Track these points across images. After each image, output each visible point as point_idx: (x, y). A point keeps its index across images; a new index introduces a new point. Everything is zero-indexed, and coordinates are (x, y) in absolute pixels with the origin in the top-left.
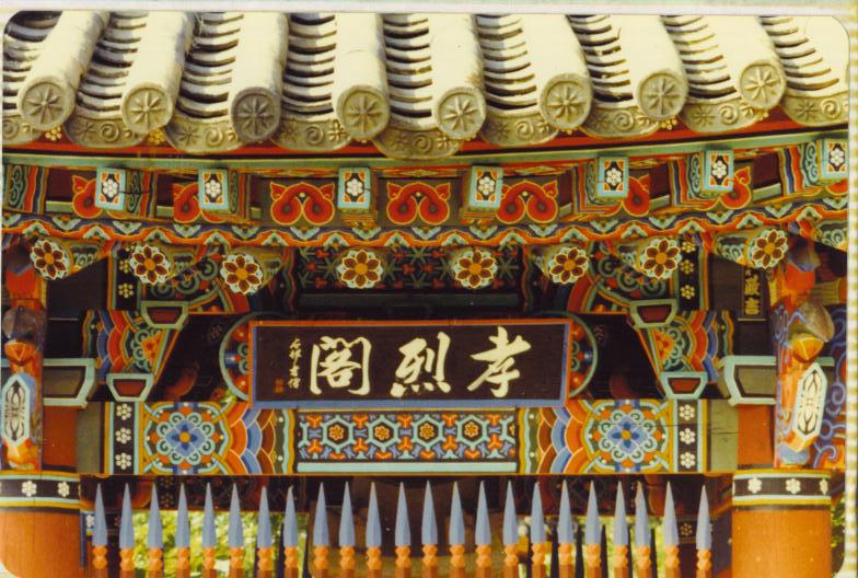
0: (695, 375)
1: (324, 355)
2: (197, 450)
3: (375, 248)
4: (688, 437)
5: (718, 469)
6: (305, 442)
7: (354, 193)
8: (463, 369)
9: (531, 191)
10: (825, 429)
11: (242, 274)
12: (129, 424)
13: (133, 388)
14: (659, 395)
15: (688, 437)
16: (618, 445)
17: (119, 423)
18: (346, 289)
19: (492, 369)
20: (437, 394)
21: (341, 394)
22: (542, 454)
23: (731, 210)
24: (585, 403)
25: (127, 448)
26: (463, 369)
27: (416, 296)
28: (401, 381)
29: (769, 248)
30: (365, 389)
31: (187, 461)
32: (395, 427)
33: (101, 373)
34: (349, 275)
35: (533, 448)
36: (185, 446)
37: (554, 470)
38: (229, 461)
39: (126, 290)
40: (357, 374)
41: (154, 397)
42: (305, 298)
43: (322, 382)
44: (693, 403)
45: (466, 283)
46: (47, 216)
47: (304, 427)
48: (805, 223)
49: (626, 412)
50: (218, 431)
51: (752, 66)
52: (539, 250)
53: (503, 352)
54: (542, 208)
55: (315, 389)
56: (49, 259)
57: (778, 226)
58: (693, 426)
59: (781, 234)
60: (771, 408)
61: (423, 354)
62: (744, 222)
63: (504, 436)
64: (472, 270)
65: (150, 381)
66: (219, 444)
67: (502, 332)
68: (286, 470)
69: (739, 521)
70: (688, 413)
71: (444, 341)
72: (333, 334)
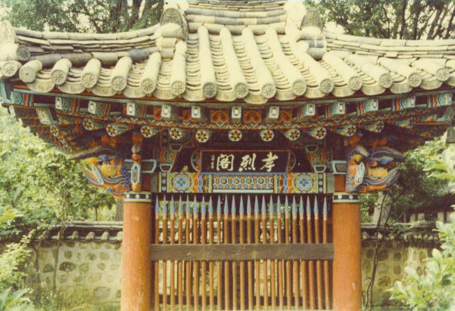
0: (322, 166)
1: (221, 159)
2: (307, 186)
3: (240, 130)
4: (321, 183)
5: (329, 192)
6: (215, 184)
7: (236, 114)
8: (259, 164)
9: (284, 114)
10: (364, 182)
11: (175, 134)
12: (166, 178)
13: (166, 168)
14: (312, 171)
15: (321, 183)
16: (301, 186)
17: (163, 178)
18: (231, 141)
19: (267, 163)
20: (252, 171)
21: (225, 170)
22: (280, 187)
23: (224, 123)
24: (292, 174)
25: (164, 185)
26: (259, 164)
27: (251, 143)
28: (242, 167)
29: (351, 131)
30: (232, 169)
31: (182, 189)
32: (240, 180)
33: (158, 164)
34: (232, 137)
35: (278, 186)
36: (181, 185)
37: (284, 192)
38: (194, 189)
39: (165, 141)
40: (230, 165)
41: (172, 171)
42: (220, 142)
43: (220, 167)
44: (322, 174)
45: (265, 140)
46: (146, 119)
47: (215, 179)
48: (361, 124)
49: (304, 176)
50: (191, 180)
51: (353, 78)
52: (286, 130)
53: (271, 159)
54: (287, 118)
55: (218, 169)
56: (146, 131)
57: (354, 124)
58: (322, 180)
59: (355, 127)
60: (345, 175)
61: (248, 159)
62: (344, 123)
63: (270, 183)
64: (266, 135)
65: (172, 166)
66: (191, 184)
67: (271, 154)
68: (210, 191)
69: (335, 207)
70: (321, 177)
71: (254, 156)
72: (224, 153)
